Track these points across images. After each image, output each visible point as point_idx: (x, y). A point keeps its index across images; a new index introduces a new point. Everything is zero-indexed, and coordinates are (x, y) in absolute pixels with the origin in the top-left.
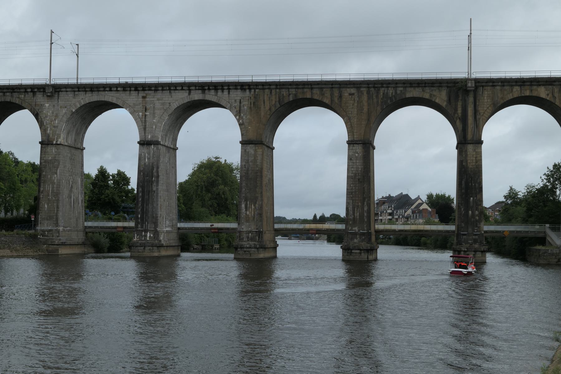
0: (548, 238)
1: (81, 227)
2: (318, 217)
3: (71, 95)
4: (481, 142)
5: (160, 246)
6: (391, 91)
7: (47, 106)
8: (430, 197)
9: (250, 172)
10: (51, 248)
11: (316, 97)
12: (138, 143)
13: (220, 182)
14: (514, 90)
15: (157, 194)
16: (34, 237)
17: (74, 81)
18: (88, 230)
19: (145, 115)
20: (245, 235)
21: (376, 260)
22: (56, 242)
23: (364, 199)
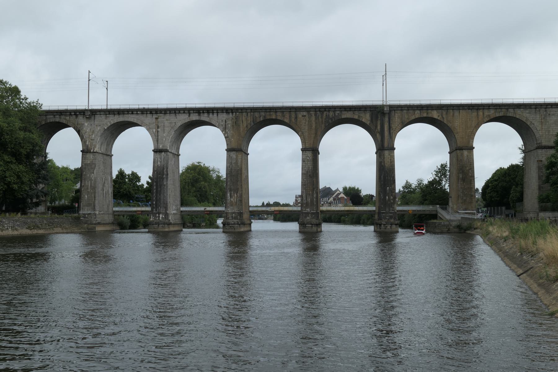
0: (439, 215)
1: (111, 211)
2: (265, 204)
3: (103, 117)
4: (394, 149)
5: (169, 224)
6: (331, 114)
7: (86, 125)
8: (345, 189)
9: (233, 171)
10: (90, 226)
11: (279, 118)
12: (153, 151)
13: (202, 179)
14: (416, 113)
15: (167, 187)
16: (78, 218)
17: (104, 107)
18: (115, 213)
19: (158, 131)
20: (230, 216)
21: (321, 231)
22: (94, 222)
23: (314, 189)
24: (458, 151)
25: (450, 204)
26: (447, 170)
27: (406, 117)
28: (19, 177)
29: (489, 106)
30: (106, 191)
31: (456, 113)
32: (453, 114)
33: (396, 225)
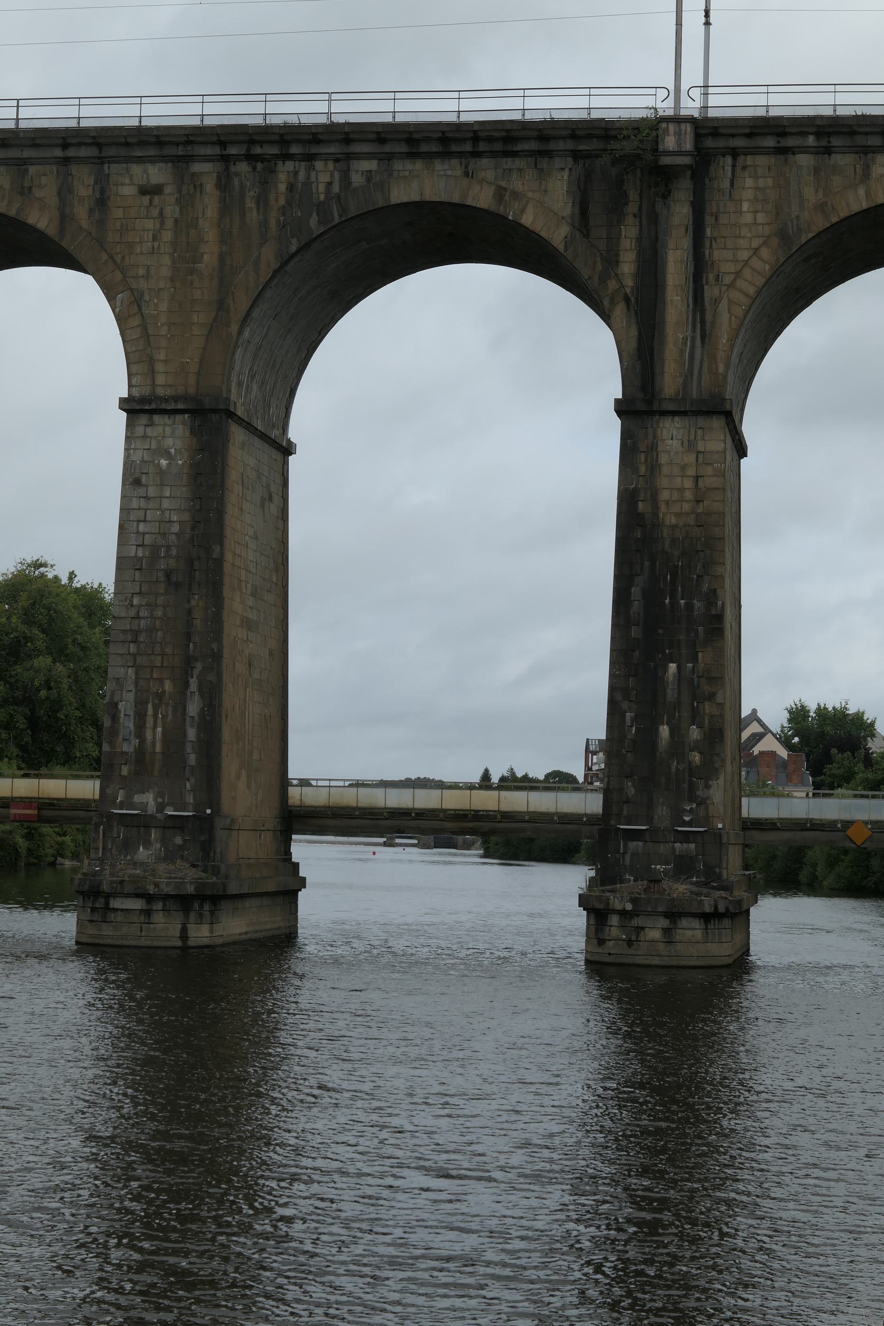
6: (324, 176)
8: (798, 715)
23: (188, 662)
27: (811, 196)
33: (706, 918)
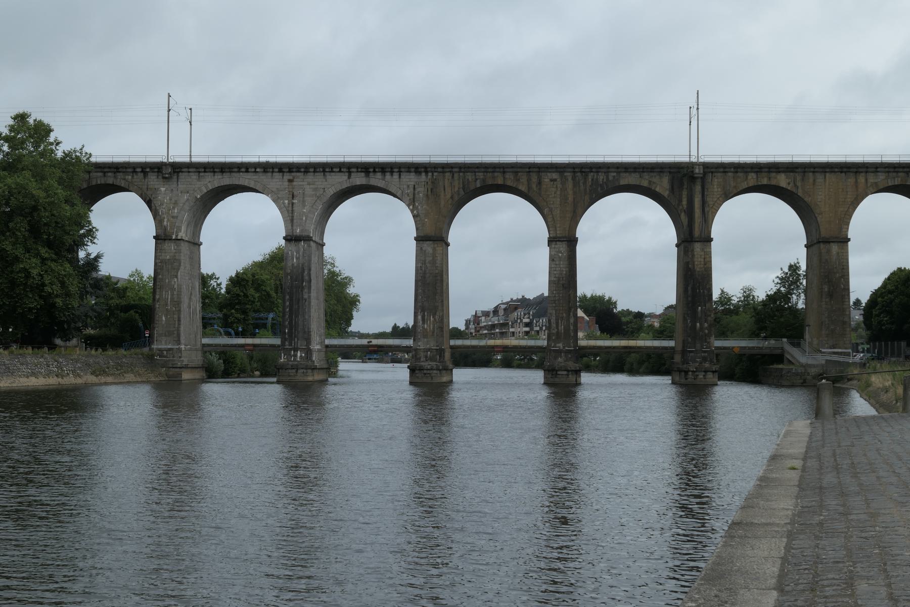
1: (199, 346)
3: (194, 176)
4: (711, 240)
5: (314, 369)
6: (601, 177)
7: (164, 192)
9: (428, 275)
10: (172, 371)
11: (509, 183)
14: (750, 177)
15: (310, 302)
17: (187, 160)
18: (205, 349)
19: (293, 204)
20: (422, 354)
22: (179, 364)
23: (570, 309)
24: (822, 245)
25: (807, 336)
26: (799, 275)
27: (732, 184)
28: (63, 284)
29: (877, 168)
30: (191, 308)
31: (820, 178)
32: (814, 180)
